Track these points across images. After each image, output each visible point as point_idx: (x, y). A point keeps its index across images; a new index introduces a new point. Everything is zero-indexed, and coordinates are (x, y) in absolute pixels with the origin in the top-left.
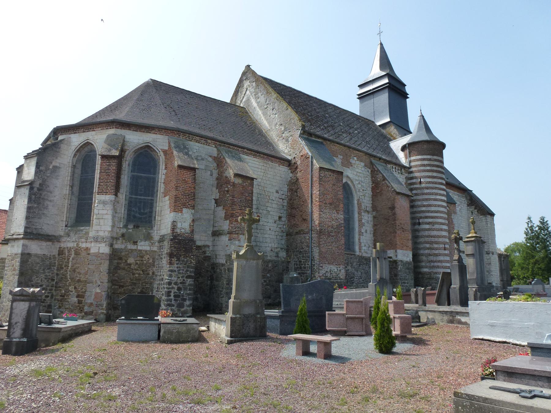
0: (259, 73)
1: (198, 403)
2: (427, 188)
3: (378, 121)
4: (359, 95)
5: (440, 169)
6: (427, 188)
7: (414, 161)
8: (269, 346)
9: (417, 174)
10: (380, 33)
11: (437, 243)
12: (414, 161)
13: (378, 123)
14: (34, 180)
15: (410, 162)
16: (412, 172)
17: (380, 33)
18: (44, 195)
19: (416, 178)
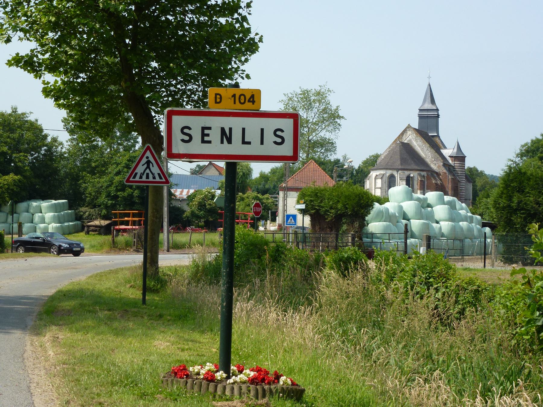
0: (421, 104)
1: (111, 396)
2: (460, 176)
3: (431, 133)
4: (419, 115)
5: (463, 170)
6: (460, 176)
7: (456, 164)
8: (446, 258)
9: (457, 170)
10: (429, 77)
11: (462, 197)
12: (456, 164)
13: (430, 135)
14: (479, 234)
15: (454, 164)
16: (455, 168)
17: (429, 77)
18: (56, 239)
19: (456, 171)
